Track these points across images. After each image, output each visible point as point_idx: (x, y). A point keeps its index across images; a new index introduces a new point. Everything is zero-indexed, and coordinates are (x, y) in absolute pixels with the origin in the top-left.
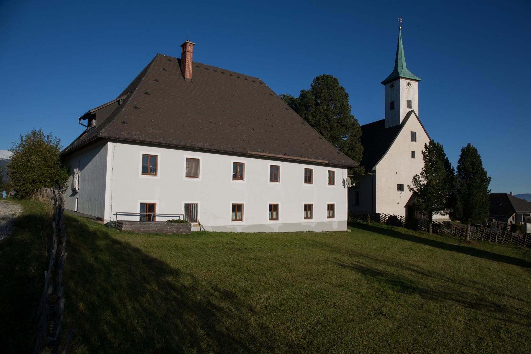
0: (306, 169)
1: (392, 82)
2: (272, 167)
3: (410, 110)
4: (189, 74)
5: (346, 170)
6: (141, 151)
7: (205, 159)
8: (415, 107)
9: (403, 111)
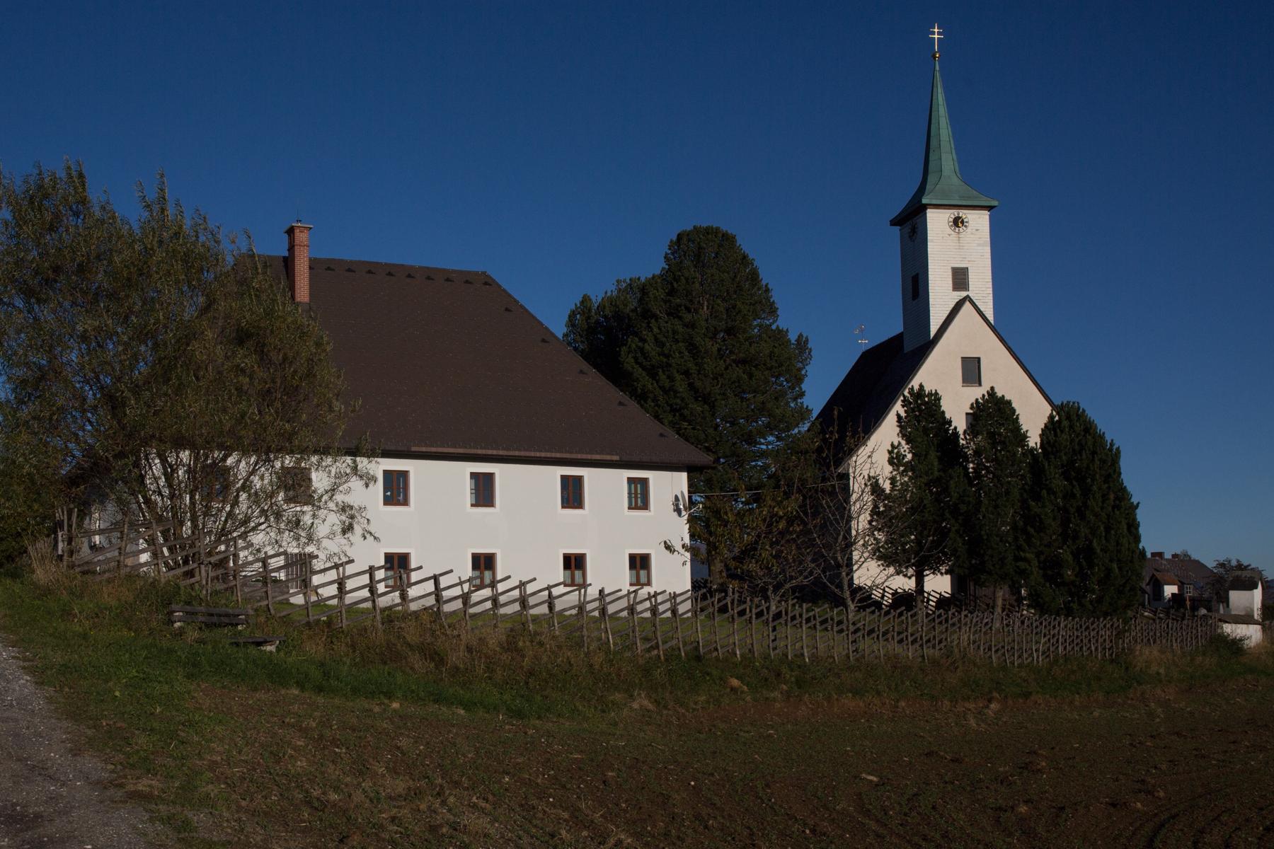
0: (563, 477)
1: (911, 222)
2: (564, 479)
3: (964, 294)
4: (303, 292)
5: (684, 475)
6: (556, 473)
7: (418, 471)
8: (982, 287)
9: (941, 297)
